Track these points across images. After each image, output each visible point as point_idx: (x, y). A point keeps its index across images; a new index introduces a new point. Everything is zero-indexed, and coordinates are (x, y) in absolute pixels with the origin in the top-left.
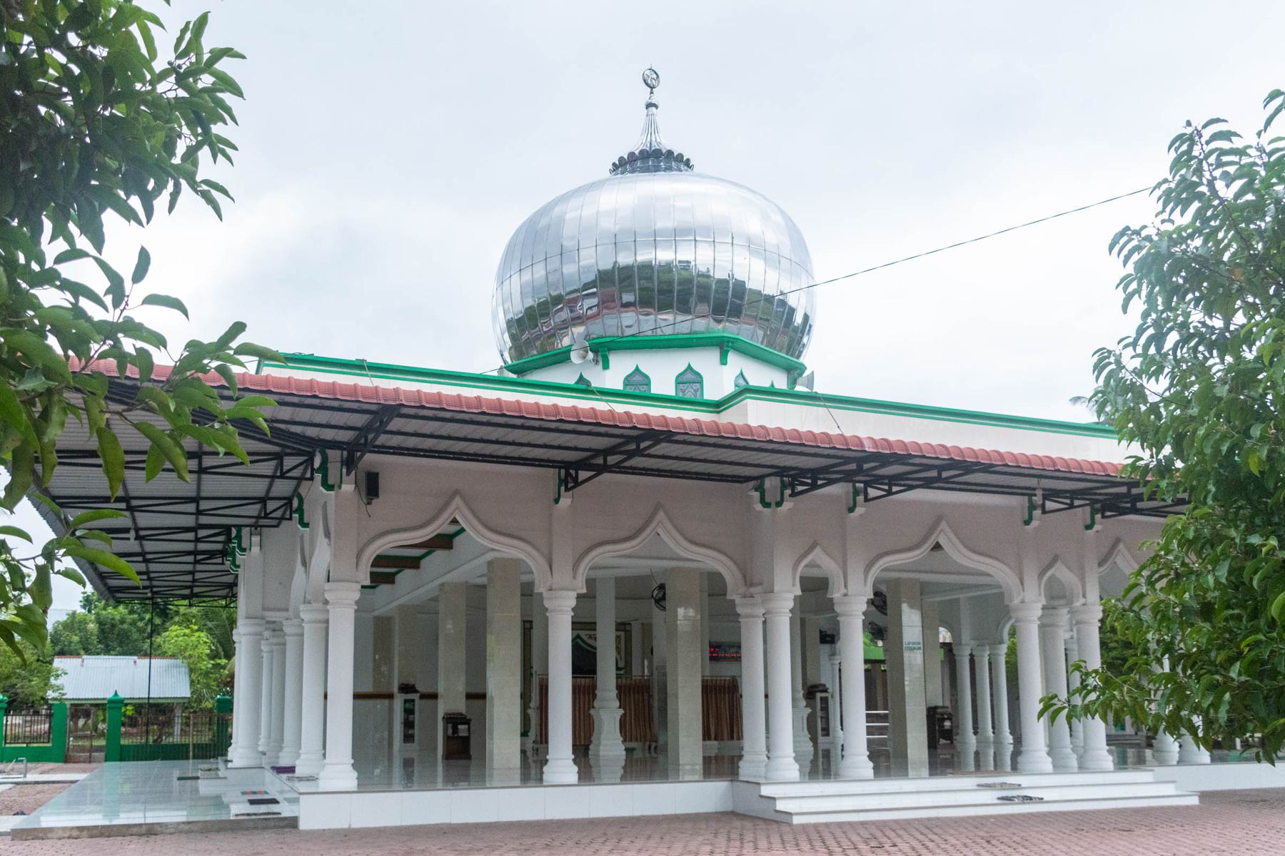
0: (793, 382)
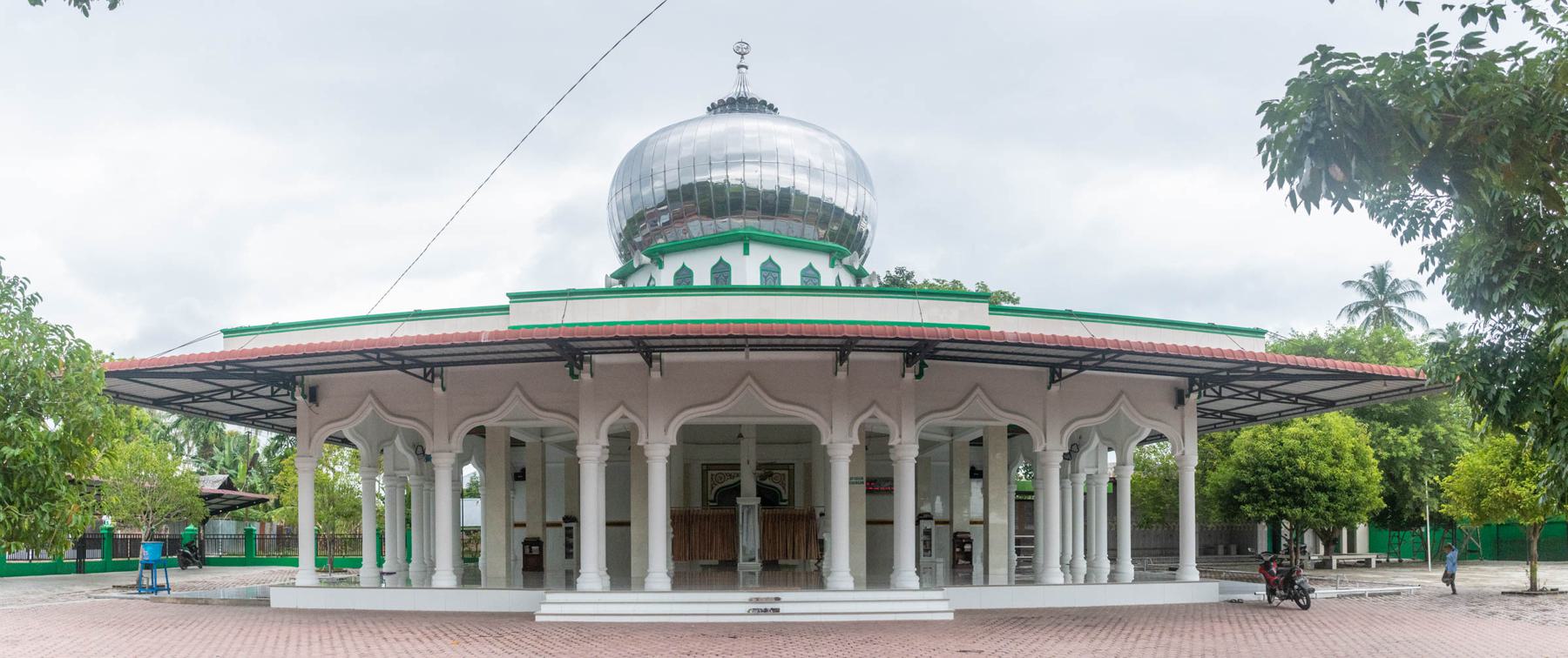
0: (858, 282)
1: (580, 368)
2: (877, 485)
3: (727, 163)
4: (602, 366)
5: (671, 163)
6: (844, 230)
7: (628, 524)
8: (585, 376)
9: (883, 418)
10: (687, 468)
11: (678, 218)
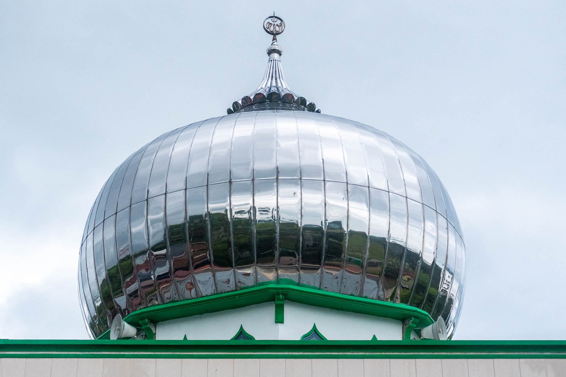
3: (254, 185)
5: (176, 183)
6: (421, 288)
11: (183, 267)
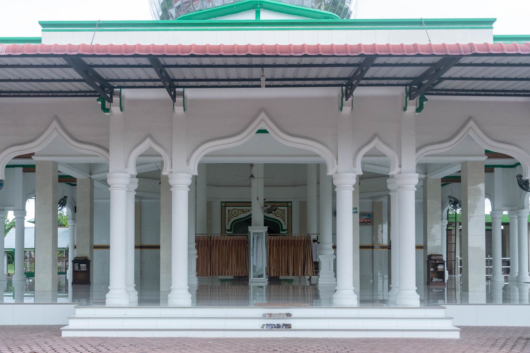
1: (111, 100)
2: (373, 214)
4: (133, 102)
7: (158, 247)
8: (115, 109)
9: (384, 148)
10: (209, 205)
